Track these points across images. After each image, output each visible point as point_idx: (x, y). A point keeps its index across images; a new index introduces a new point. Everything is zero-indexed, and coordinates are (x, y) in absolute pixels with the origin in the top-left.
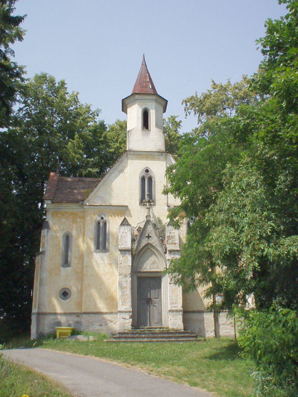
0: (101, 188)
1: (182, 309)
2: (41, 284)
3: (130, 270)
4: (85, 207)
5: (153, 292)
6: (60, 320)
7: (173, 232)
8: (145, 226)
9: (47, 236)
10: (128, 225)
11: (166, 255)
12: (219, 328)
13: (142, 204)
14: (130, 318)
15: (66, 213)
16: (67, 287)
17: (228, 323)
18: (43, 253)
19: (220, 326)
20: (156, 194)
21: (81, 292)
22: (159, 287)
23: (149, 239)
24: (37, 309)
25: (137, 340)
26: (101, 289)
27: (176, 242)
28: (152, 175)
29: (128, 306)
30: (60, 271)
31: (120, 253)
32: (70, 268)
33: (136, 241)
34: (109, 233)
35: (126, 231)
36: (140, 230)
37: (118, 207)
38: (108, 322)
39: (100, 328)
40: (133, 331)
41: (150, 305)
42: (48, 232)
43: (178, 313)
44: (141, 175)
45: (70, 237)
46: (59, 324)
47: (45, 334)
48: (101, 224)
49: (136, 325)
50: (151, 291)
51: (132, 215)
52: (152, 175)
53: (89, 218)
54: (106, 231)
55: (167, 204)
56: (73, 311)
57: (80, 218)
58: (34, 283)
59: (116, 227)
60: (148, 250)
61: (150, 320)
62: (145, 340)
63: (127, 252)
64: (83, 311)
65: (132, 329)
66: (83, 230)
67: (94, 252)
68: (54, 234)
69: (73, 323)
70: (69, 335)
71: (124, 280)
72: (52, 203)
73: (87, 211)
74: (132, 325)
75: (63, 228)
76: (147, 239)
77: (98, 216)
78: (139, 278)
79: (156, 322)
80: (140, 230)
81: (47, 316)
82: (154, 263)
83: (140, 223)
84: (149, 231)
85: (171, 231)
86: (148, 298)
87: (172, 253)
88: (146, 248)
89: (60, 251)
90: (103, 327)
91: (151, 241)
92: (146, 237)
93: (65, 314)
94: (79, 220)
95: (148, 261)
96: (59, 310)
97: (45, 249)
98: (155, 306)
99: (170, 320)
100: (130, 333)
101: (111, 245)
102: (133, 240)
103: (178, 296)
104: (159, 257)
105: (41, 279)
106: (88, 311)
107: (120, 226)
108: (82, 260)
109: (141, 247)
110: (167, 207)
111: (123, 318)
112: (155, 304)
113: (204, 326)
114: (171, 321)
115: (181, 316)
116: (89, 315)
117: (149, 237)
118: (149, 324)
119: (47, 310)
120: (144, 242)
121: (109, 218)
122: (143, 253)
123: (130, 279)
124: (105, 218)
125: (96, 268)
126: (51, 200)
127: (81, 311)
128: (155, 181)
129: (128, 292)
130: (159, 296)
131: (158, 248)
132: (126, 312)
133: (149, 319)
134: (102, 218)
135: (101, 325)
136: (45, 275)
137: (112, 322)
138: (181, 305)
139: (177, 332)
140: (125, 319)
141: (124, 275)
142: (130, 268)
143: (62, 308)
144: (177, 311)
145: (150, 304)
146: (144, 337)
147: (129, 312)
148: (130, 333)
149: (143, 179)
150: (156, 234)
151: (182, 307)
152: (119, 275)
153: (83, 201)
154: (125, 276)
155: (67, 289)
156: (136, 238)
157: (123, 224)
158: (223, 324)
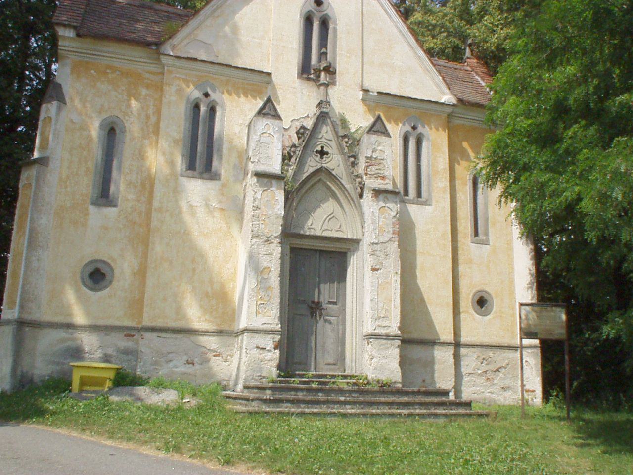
0: (208, 22)
1: (399, 332)
2: (32, 243)
3: (281, 228)
4: (164, 59)
5: (325, 287)
6: (79, 342)
7: (379, 148)
8: (316, 126)
9: (57, 120)
10: (277, 117)
11: (362, 201)
12: (462, 382)
13: (305, 76)
14: (275, 349)
15: (114, 69)
16: (103, 259)
17: (479, 372)
18: (43, 162)
19: (463, 378)
20: (338, 59)
21: (142, 273)
22: (341, 276)
23: (322, 158)
24: (17, 308)
25: (324, 409)
26: (194, 270)
27: (386, 173)
28: (328, 12)
29: (271, 318)
30: (87, 214)
31: (258, 181)
32: (114, 209)
33: (293, 160)
34: (221, 138)
35: (271, 131)
36: (303, 134)
37: (247, 74)
38: (210, 355)
39: (189, 369)
40: (281, 382)
41: (318, 318)
42: (59, 110)
43: (389, 342)
44: (305, 11)
45: (117, 132)
46: (77, 353)
47: (36, 380)
48: (203, 109)
49: (287, 367)
50: (322, 285)
51: (281, 99)
52: (330, 14)
53: (173, 89)
54: (213, 126)
55: (362, 86)
56: (117, 323)
57: (148, 87)
58: (10, 240)
59: (241, 122)
60: (320, 185)
61: (316, 354)
62: (349, 410)
63: (274, 182)
64: (146, 322)
65: (280, 376)
66: (153, 119)
67: (181, 175)
68: (75, 117)
69: (114, 354)
70: (109, 384)
71: (263, 250)
72: (78, 35)
73: (170, 72)
74: (279, 367)
75: (102, 106)
76: (318, 159)
77: (196, 88)
78: (293, 250)
79: (331, 361)
80: (303, 134)
81: (47, 331)
82: (331, 217)
83: (298, 120)
84: (323, 140)
85: (369, 146)
86: (313, 302)
87: (381, 197)
88: (316, 179)
89: (89, 163)
90: (197, 366)
91: (328, 165)
92: (317, 152)
93: (94, 328)
94: (144, 91)
95: (319, 211)
96: (80, 318)
97: (47, 154)
98: (330, 323)
99: (372, 359)
100: (302, 390)
101: (224, 166)
102: (286, 158)
103: (390, 301)
104: (344, 205)
105: (32, 230)
106: (159, 323)
107: (255, 116)
108: (147, 194)
109: (304, 176)
110: (362, 93)
111: (258, 348)
112: (327, 317)
113: (433, 377)
114: (374, 360)
115: (397, 351)
116: (160, 335)
117: (322, 153)
118: (313, 367)
119: (45, 314)
120: (312, 164)
121: (223, 96)
122: (306, 192)
123: (280, 249)
124: (214, 96)
125: (187, 218)
126: (75, 28)
127: (140, 322)
128: (335, 29)
129: (274, 280)
130: (340, 299)
131: (343, 182)
132: (266, 332)
133: (313, 354)
134: (206, 95)
135: (190, 363)
136: (45, 221)
137: (218, 356)
138: (398, 324)
139: (385, 388)
140: (263, 349)
141: (265, 239)
142: (281, 221)
143: (88, 313)
144: (387, 337)
145: (318, 316)
146: (345, 403)
147: (274, 332)
148: (302, 390)
149: (308, 20)
150: (340, 146)
151: (400, 328)
152: (252, 237)
153: (158, 44)
154: (268, 241)
155: (104, 262)
156: (294, 152)
157: (264, 112)
158: (470, 374)
